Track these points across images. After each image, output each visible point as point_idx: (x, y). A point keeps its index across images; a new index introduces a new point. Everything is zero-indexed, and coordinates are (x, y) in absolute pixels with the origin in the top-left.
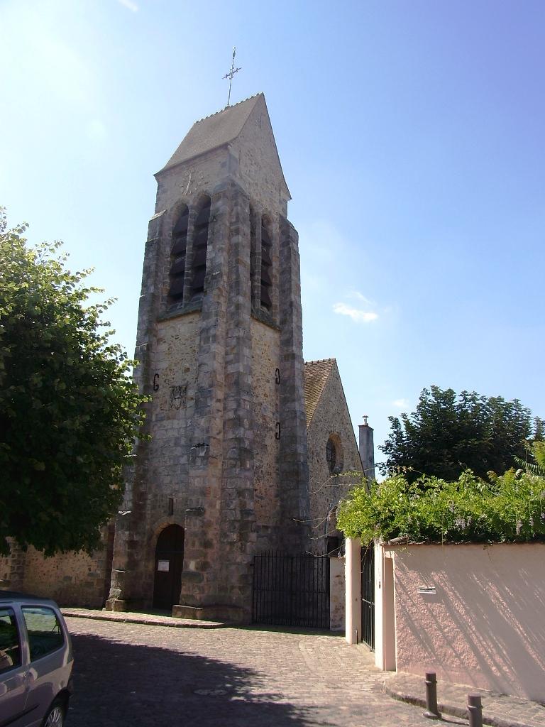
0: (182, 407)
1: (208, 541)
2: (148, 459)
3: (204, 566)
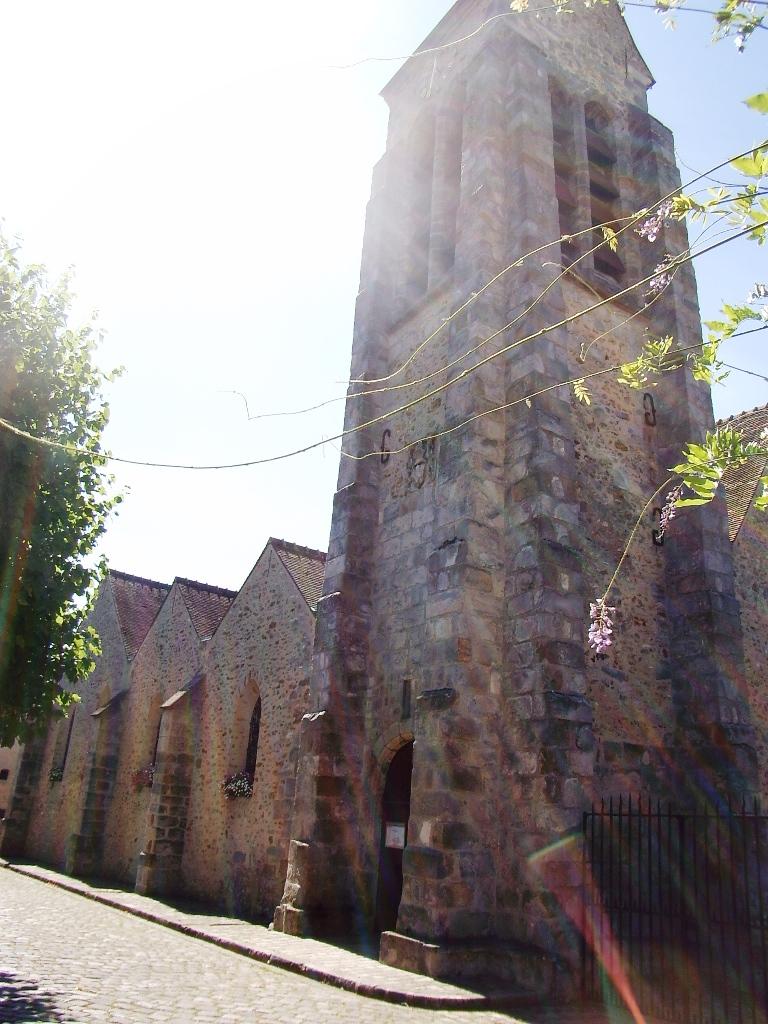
0: (428, 479)
1: (466, 771)
2: (370, 604)
3: (452, 835)
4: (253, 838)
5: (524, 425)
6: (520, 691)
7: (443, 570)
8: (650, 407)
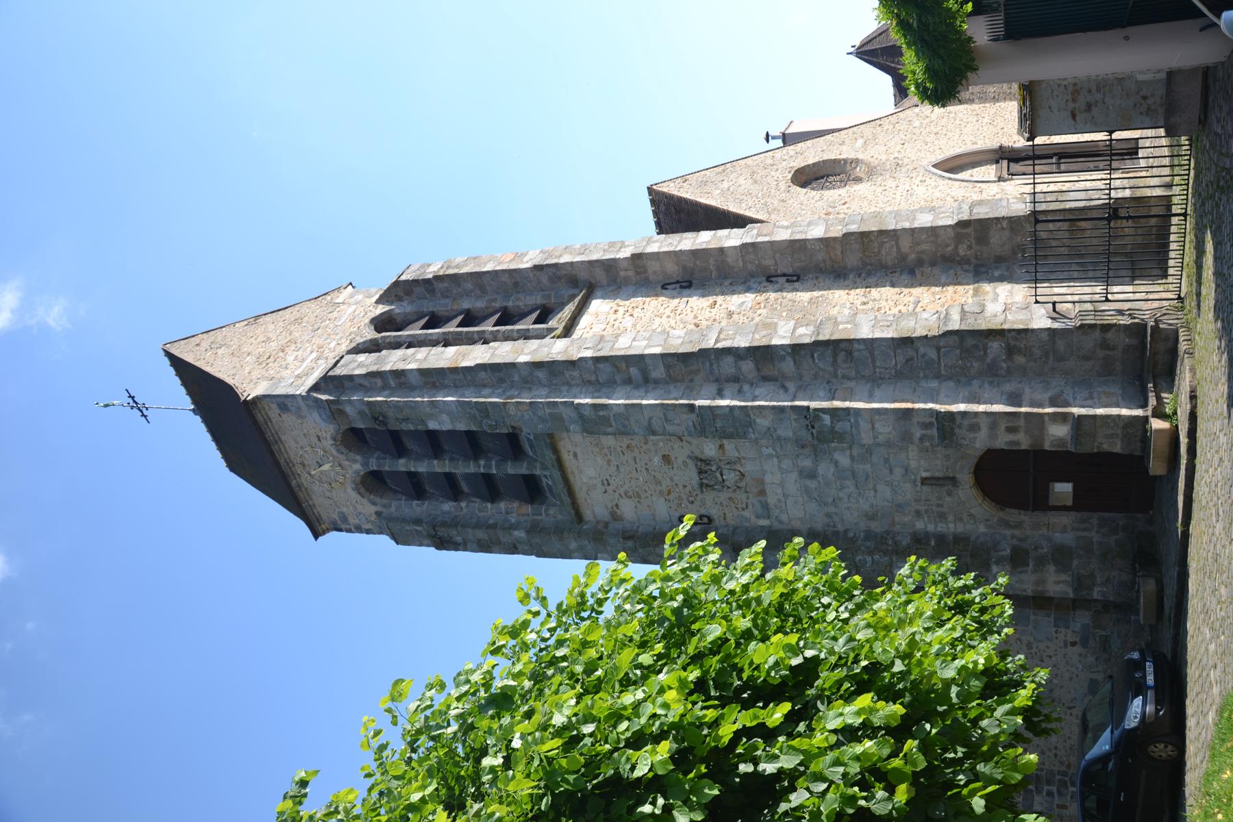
0: (738, 467)
4: (1074, 669)
5: (708, 363)
6: (936, 359)
7: (833, 427)
8: (674, 286)
